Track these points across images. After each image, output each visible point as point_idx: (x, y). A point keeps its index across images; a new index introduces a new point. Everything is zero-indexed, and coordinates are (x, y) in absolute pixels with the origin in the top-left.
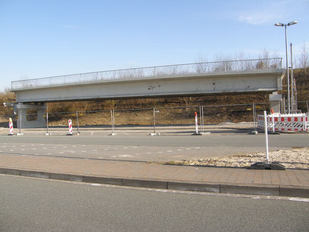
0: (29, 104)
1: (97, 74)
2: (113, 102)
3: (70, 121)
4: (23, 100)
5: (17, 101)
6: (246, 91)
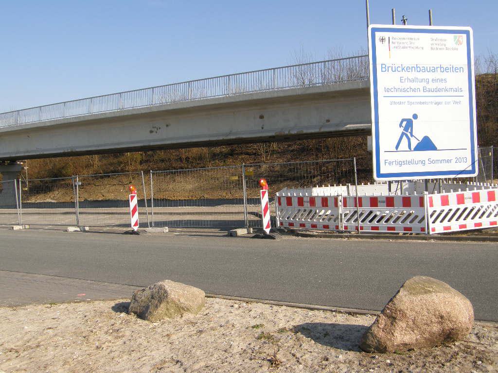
1: (121, 96)
2: (138, 156)
6: (323, 130)
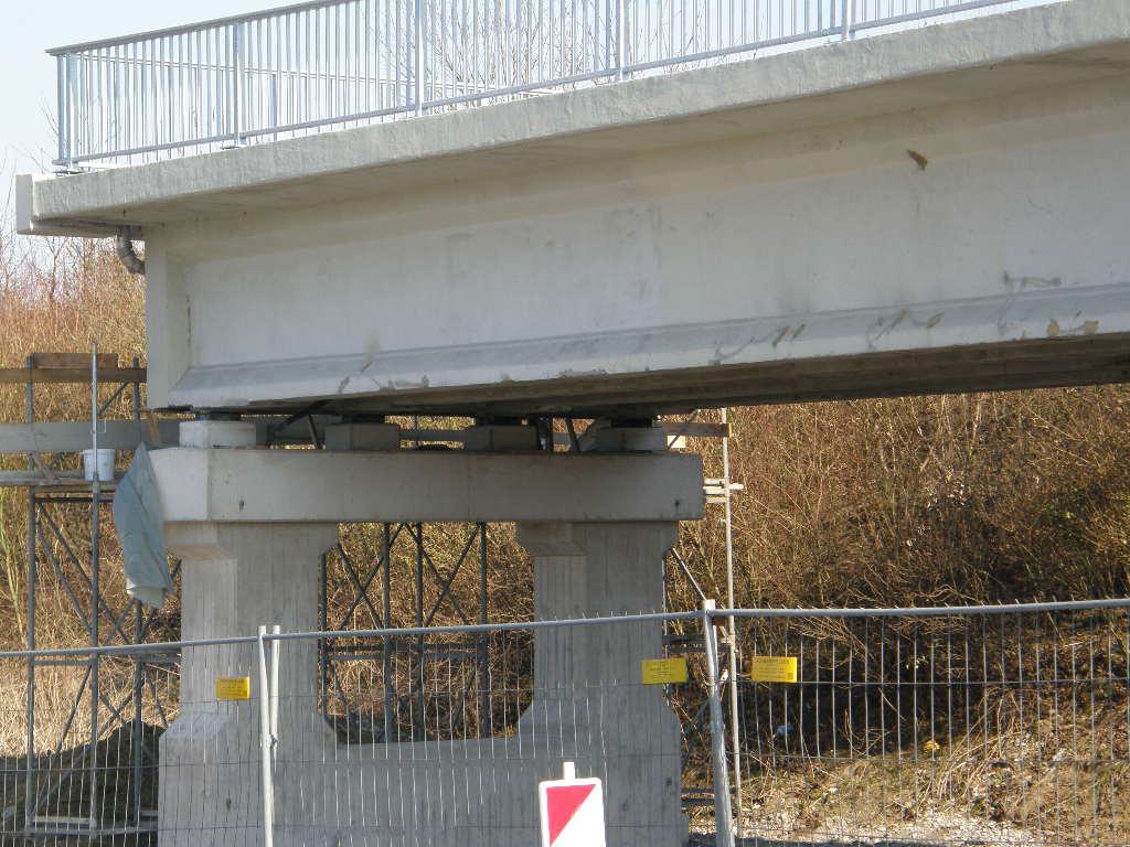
0: (366, 432)
3: (566, 804)
4: (241, 372)
5: (159, 393)
